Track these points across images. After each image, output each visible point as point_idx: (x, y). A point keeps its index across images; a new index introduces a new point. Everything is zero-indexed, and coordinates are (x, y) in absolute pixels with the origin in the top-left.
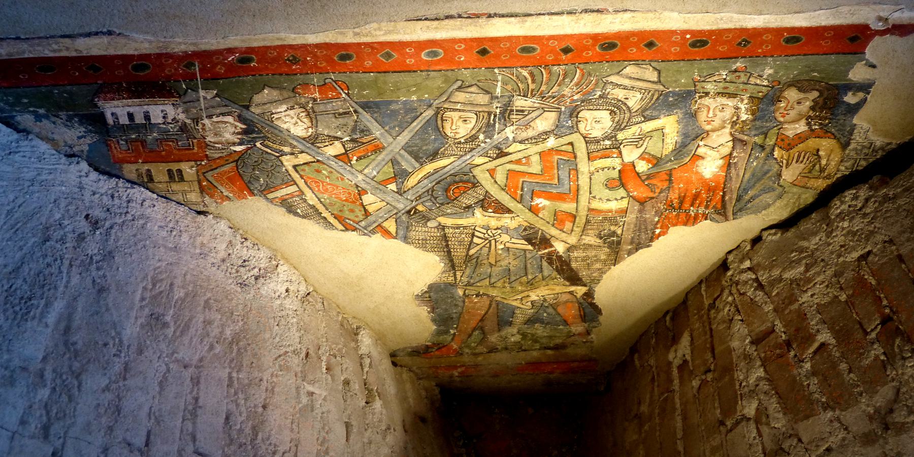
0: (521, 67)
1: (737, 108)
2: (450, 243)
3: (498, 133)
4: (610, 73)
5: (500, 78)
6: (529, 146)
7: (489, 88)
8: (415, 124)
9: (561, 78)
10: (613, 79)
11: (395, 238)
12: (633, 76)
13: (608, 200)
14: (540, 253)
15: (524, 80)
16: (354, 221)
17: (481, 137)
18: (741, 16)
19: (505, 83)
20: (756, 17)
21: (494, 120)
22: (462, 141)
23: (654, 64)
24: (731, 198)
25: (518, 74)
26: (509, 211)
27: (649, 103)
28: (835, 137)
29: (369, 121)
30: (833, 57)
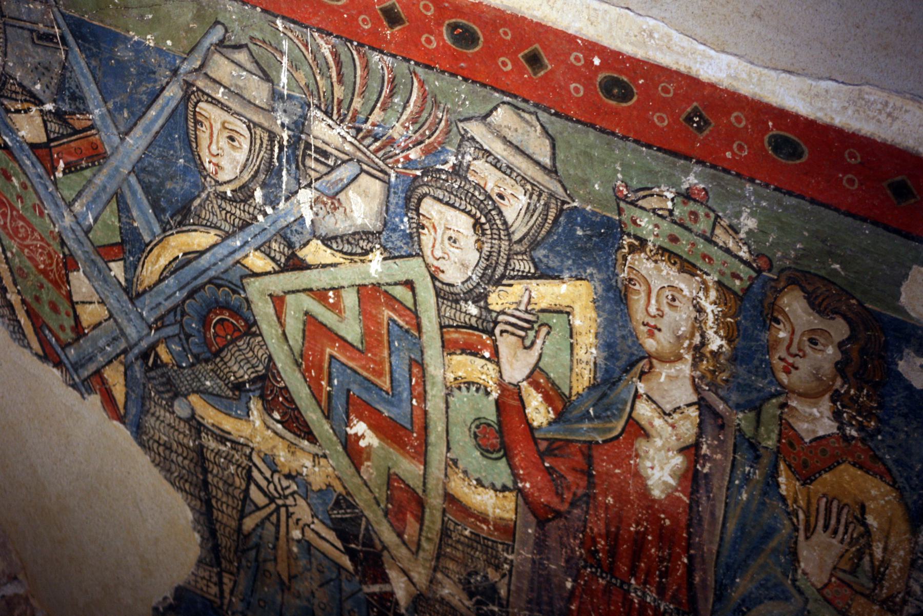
0: (319, 30)
1: (700, 310)
2: (210, 477)
3: (287, 199)
4: (471, 113)
5: (285, 45)
6: (338, 258)
7: (269, 67)
8: (153, 112)
9: (386, 91)
10: (475, 129)
11: (121, 419)
12: (510, 136)
13: (480, 483)
14: (366, 589)
15: (325, 70)
16: (58, 339)
17: (258, 194)
18: (686, 42)
19: (294, 65)
20: (712, 53)
21: (279, 159)
22: (228, 190)
23: (543, 116)
24: (704, 581)
25: (315, 47)
26: (313, 439)
27: (542, 226)
28: (895, 482)
29: (84, 76)
30: (867, 228)
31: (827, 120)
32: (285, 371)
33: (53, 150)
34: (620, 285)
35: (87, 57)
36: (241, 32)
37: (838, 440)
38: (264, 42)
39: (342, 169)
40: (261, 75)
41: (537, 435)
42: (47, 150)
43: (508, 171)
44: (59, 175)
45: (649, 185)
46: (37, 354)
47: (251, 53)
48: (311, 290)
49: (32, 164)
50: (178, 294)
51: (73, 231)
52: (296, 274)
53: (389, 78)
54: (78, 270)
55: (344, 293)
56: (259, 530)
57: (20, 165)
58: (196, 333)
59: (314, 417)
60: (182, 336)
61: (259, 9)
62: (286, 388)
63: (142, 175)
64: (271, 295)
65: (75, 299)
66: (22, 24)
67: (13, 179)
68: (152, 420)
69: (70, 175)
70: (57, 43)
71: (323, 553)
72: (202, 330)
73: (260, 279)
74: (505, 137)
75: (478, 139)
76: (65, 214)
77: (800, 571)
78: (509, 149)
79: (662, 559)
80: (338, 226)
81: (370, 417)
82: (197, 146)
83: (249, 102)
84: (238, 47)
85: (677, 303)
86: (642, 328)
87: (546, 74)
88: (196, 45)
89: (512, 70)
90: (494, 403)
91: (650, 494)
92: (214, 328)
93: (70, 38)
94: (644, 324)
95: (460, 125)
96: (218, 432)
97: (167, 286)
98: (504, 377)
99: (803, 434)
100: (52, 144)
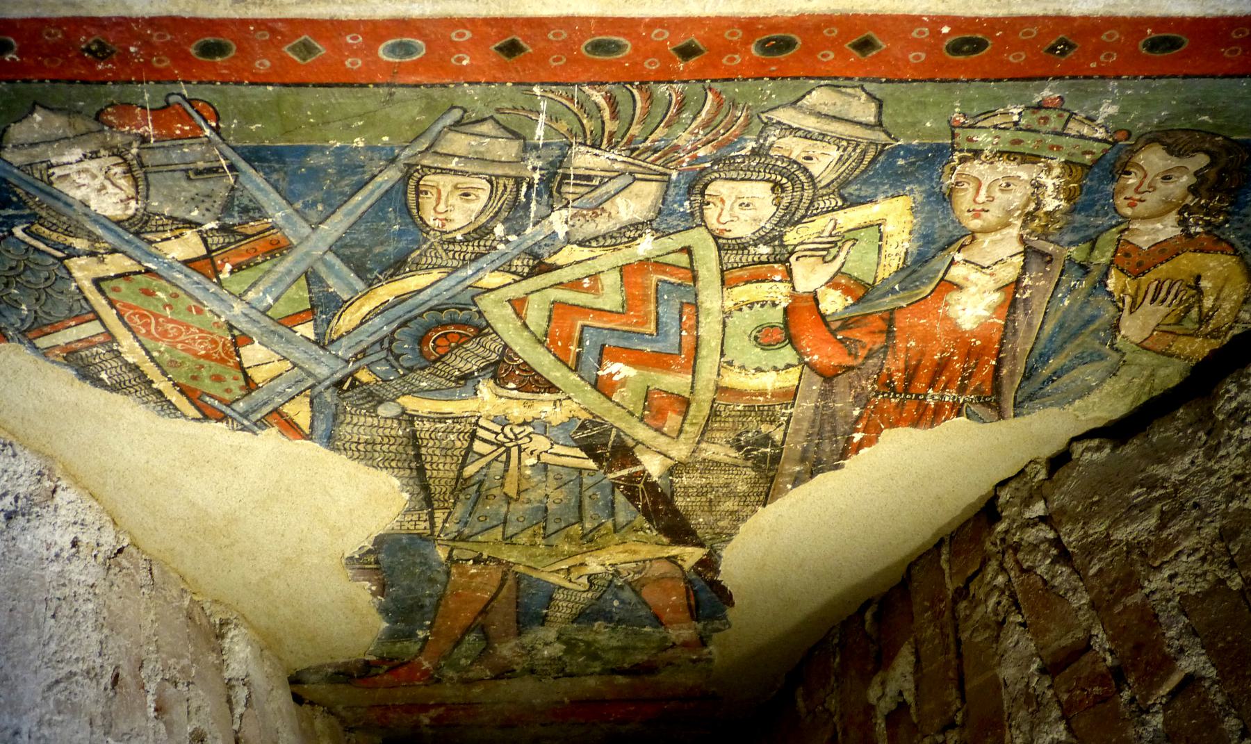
2: (423, 451)
3: (535, 224)
5: (543, 105)
6: (598, 252)
8: (358, 198)
9: (673, 110)
13: (758, 370)
19: (553, 117)
21: (528, 195)
26: (551, 388)
27: (854, 169)
31: (1219, 13)
32: (524, 352)
33: (215, 259)
34: (944, 189)
35: (266, 174)
36: (484, 108)
37: (1180, 239)
38: (515, 108)
39: (609, 184)
40: (510, 136)
41: (828, 319)
42: (209, 260)
43: (821, 137)
44: (225, 275)
45: (993, 109)
46: (194, 419)
47: (498, 122)
48: (561, 283)
49: (186, 276)
50: (385, 328)
51: (246, 315)
52: (549, 275)
53: (677, 101)
54: (253, 342)
55: (310, 230)
56: (485, 470)
57: (168, 281)
58: (408, 351)
59: (558, 374)
60: (391, 358)
61: (509, 84)
62: (525, 363)
63: (341, 251)
64: (509, 301)
65: (245, 366)
66: (173, 167)
67: (159, 293)
68: (349, 429)
69: (241, 272)
70: (225, 172)
71: (563, 466)
72: (417, 347)
73: (495, 292)
74: (819, 113)
75: (785, 122)
76: (234, 305)
77: (1119, 337)
78: (823, 121)
79: (964, 370)
80: (599, 228)
81: (629, 357)
82: (418, 210)
83: (493, 161)
84: (481, 121)
85: (1012, 187)
86: (967, 214)
87: (879, 54)
88: (424, 132)
89: (835, 59)
90: (782, 313)
91: (960, 328)
92: (434, 342)
93: (242, 165)
94: (969, 211)
95: (763, 116)
96: (436, 416)
97: (370, 326)
98: (797, 289)
99: (1141, 245)
100: (214, 254)
